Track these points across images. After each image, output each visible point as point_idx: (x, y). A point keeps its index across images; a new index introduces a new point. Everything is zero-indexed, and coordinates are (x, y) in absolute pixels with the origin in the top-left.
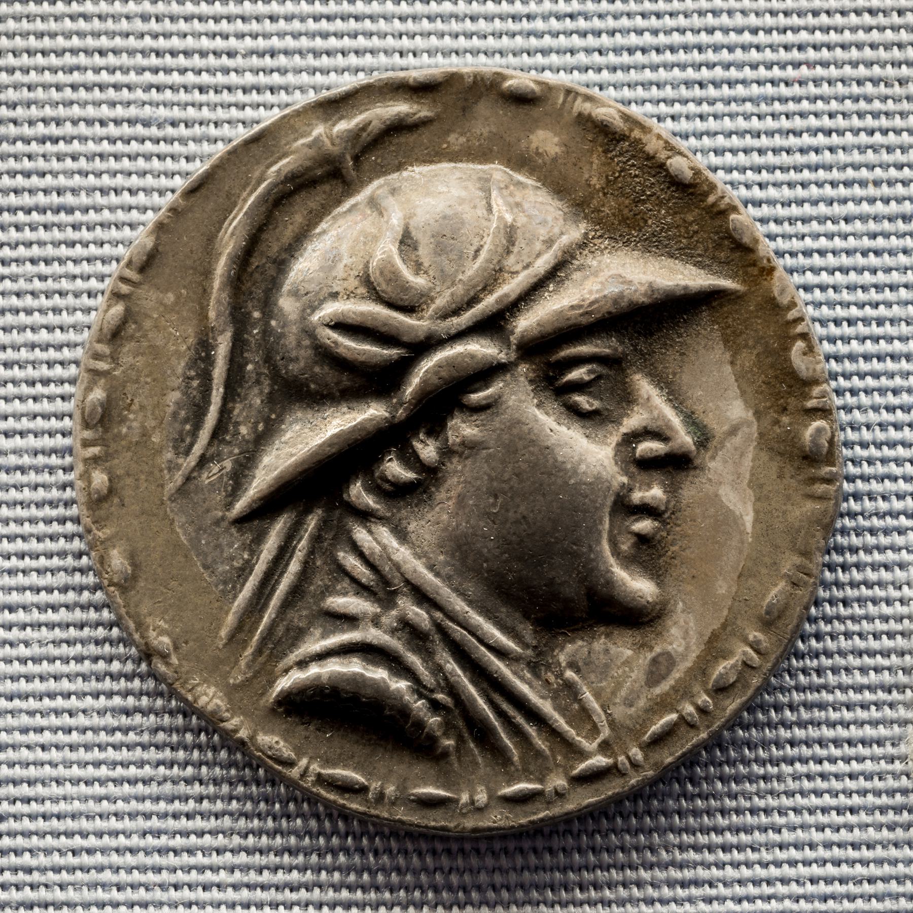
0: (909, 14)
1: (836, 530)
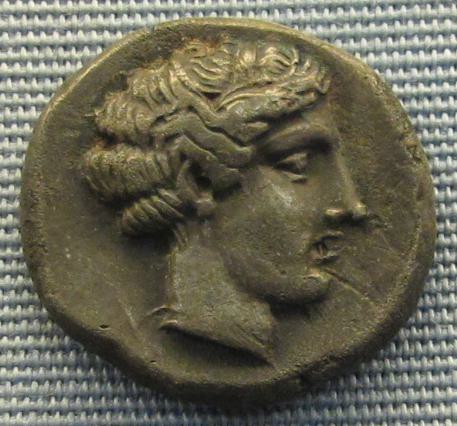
1: (431, 277)
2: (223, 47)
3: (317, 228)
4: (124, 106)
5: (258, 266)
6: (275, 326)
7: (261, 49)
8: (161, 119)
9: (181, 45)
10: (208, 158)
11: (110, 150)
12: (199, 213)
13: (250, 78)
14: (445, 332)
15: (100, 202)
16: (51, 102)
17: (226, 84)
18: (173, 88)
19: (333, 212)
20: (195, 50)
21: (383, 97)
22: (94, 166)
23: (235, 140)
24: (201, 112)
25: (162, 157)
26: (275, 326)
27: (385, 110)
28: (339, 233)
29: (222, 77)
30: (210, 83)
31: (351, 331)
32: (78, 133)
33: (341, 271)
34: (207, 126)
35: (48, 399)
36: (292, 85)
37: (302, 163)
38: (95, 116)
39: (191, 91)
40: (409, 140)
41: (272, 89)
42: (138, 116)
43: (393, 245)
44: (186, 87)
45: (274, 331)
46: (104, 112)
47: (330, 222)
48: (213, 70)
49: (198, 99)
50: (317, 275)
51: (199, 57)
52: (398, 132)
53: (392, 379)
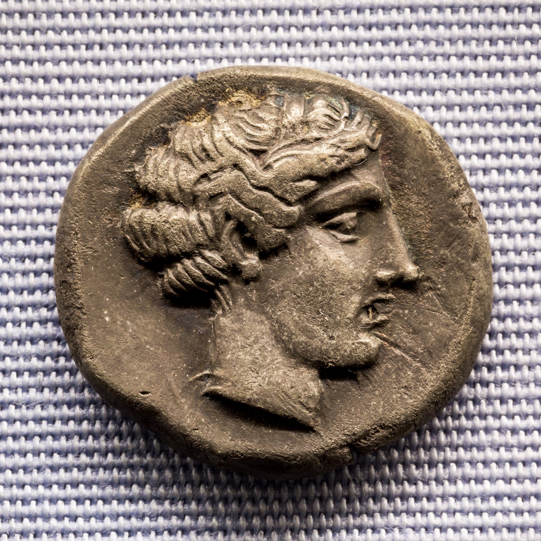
0: (538, 107)
2: (269, 99)
3: (367, 290)
4: (165, 162)
5: (305, 330)
6: (322, 394)
7: (310, 102)
8: (205, 176)
9: (225, 97)
10: (253, 219)
11: (151, 208)
12: (244, 275)
13: (297, 134)
15: (140, 262)
16: (89, 156)
17: (271, 140)
18: (218, 144)
19: (384, 274)
20: (240, 102)
21: (438, 153)
22: (134, 224)
23: (282, 199)
24: (248, 170)
25: (206, 216)
26: (322, 394)
27: (440, 165)
28: (390, 295)
29: (269, 133)
30: (255, 139)
31: (401, 398)
32: (117, 189)
33: (391, 335)
34: (252, 185)
35: (105, 455)
36: (343, 142)
37: (351, 223)
38: (135, 172)
39: (236, 147)
40: (464, 199)
41: (320, 145)
42: (181, 173)
43: (446, 309)
44: (231, 143)
45: (321, 400)
46: (145, 168)
47: (381, 284)
48: (260, 125)
49: (243, 156)
50: (367, 340)
51: (243, 111)
52: (453, 189)
53: (484, 407)
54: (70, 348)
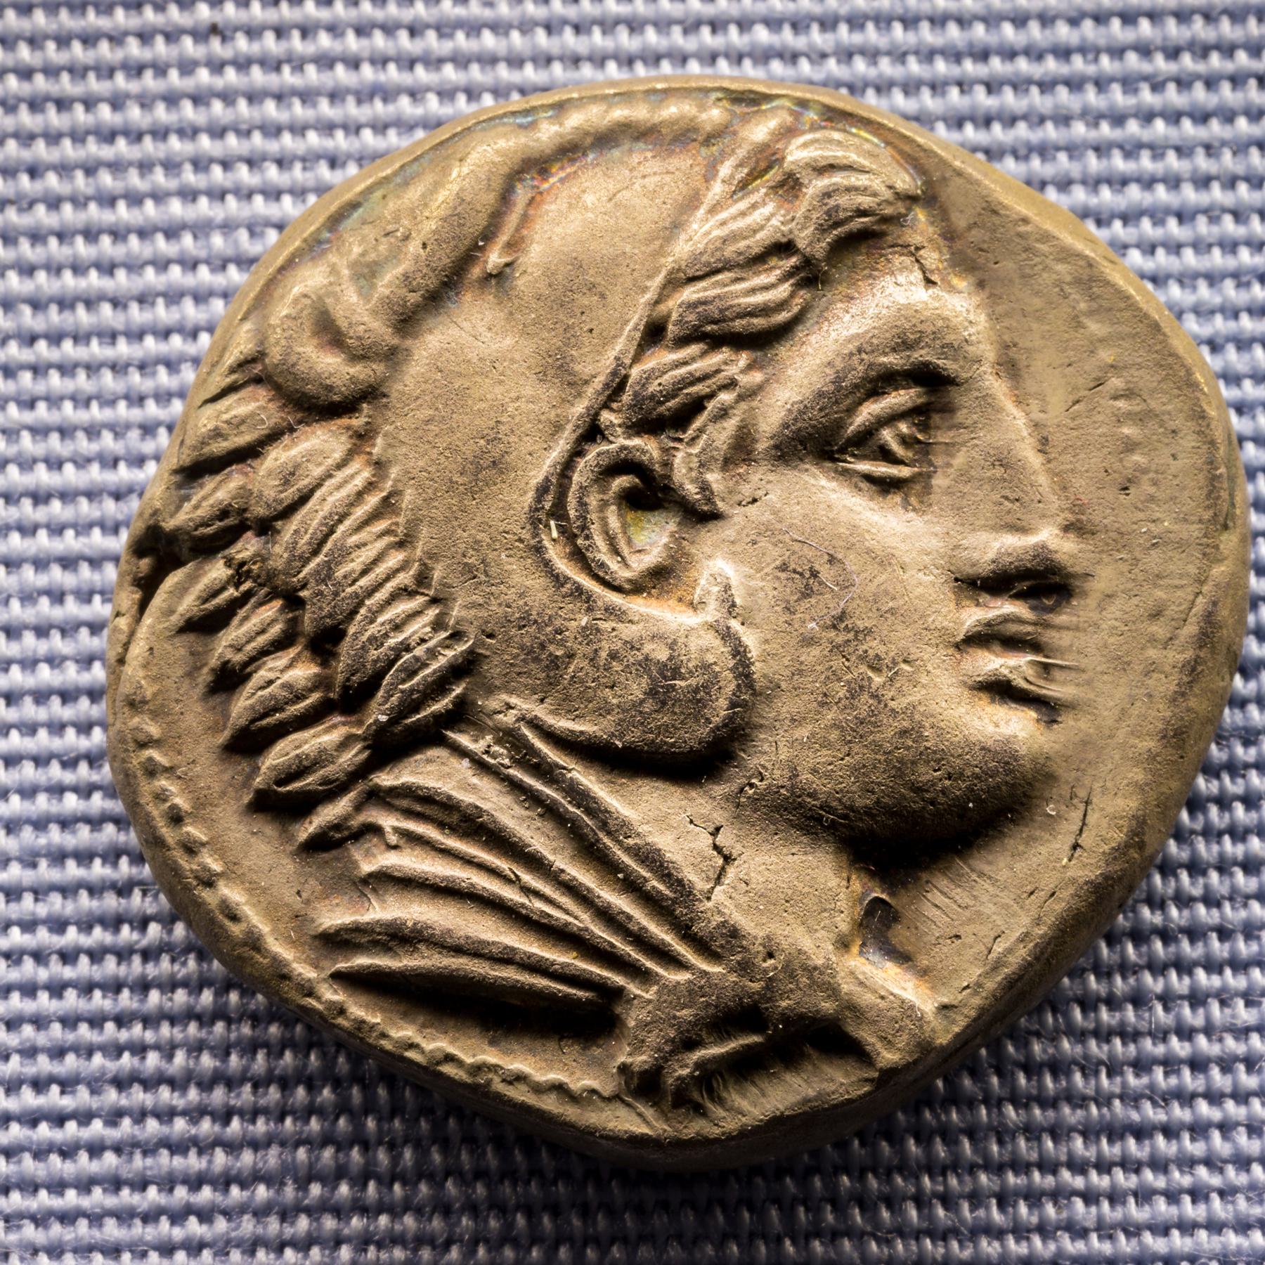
0: (1259, 411)
14: (1243, 914)
54: (139, 837)
